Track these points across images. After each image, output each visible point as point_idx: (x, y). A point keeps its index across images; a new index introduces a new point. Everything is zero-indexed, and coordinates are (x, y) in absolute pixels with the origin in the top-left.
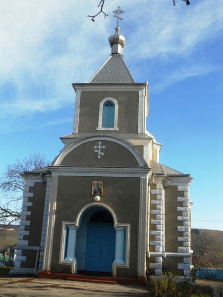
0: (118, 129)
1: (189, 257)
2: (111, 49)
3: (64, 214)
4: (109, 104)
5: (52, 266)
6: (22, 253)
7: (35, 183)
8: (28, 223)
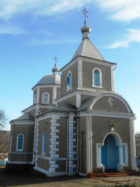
0: (102, 88)
1: (124, 162)
2: (82, 35)
3: (96, 140)
4: (97, 72)
5: (94, 170)
6: (56, 163)
7: (60, 117)
8: (58, 143)
